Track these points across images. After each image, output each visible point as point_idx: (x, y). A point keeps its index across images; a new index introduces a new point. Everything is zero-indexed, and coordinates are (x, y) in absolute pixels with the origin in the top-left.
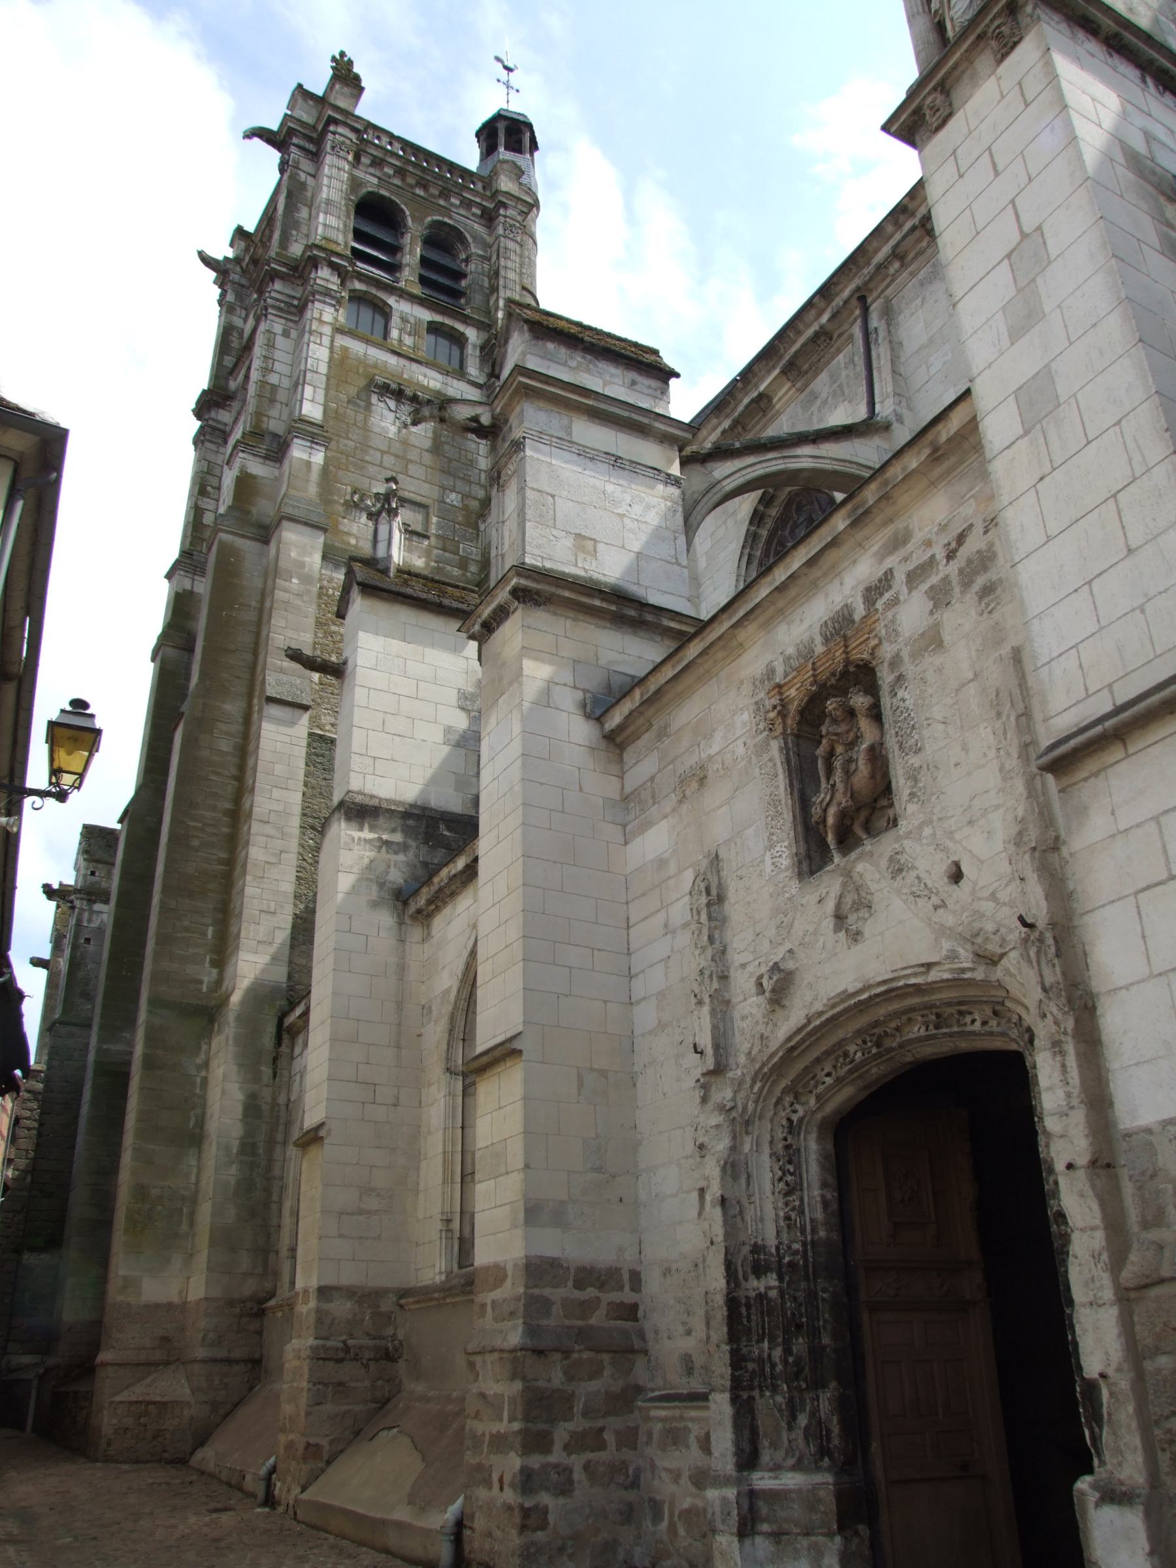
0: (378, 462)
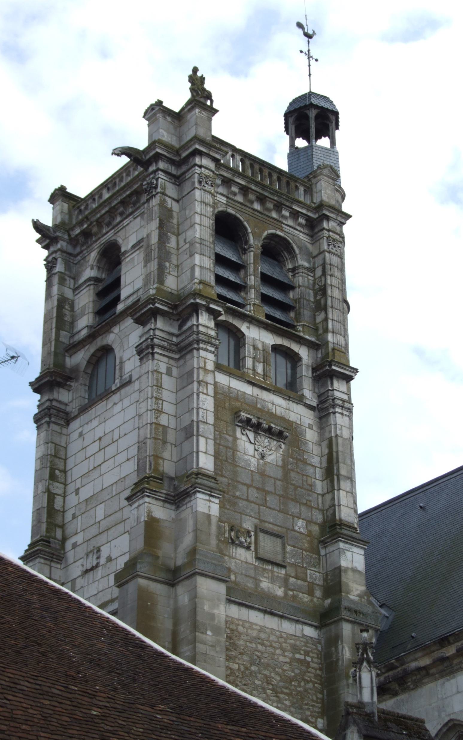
0: (245, 497)
